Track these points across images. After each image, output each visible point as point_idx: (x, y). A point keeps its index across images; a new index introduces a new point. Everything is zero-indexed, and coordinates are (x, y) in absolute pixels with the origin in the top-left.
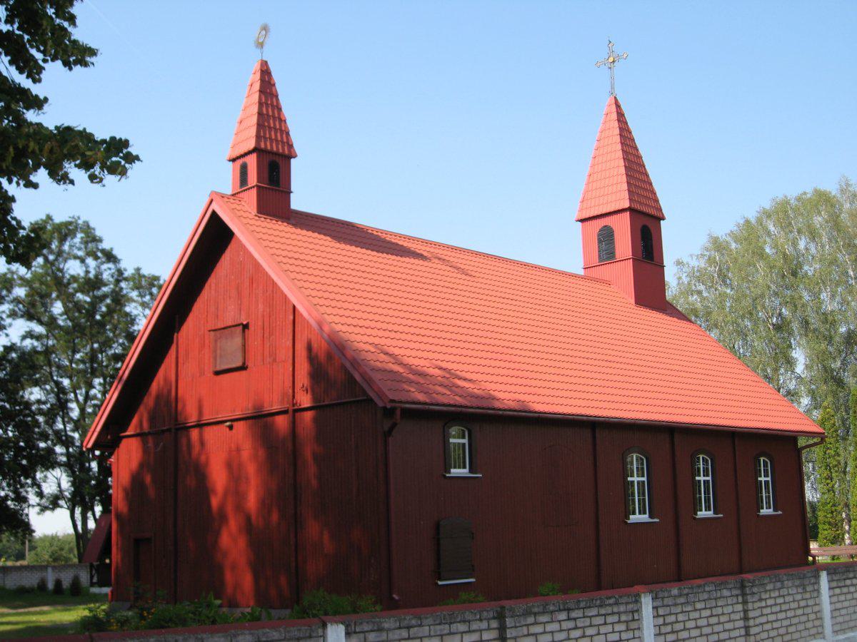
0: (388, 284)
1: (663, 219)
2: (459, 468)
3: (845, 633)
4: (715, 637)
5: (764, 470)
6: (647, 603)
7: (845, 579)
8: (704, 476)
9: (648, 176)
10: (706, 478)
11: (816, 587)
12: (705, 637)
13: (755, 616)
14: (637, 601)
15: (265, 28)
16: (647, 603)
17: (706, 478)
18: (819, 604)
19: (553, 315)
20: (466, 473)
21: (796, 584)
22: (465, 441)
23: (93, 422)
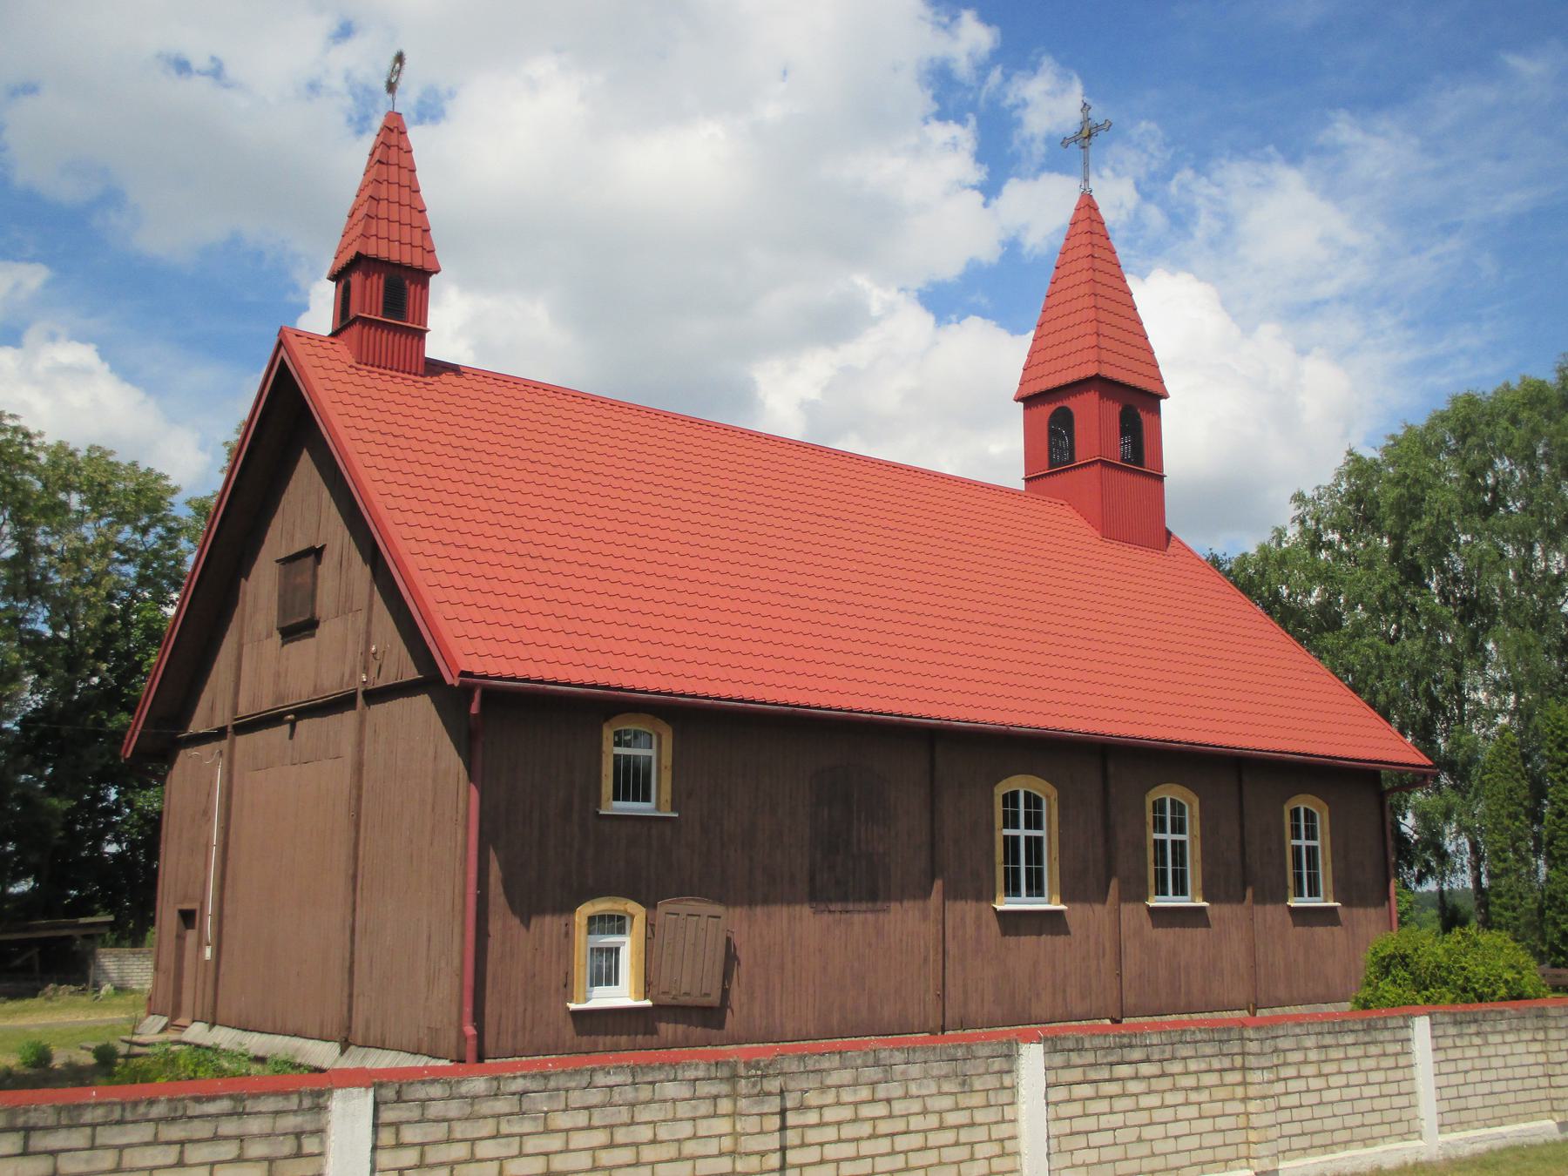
0: (975, 538)
1: (1166, 397)
2: (636, 799)
3: (1517, 1121)
4: (864, 1167)
5: (1306, 827)
6: (1032, 1058)
7: (1111, 1064)
8: (1307, 838)
9: (1140, 324)
10: (1295, 842)
11: (1007, 1081)
12: (833, 1166)
13: (764, 1148)
14: (1011, 1057)
15: (400, 58)
16: (1032, 1058)
17: (1295, 842)
18: (1013, 1121)
19: (904, 545)
20: (651, 810)
21: (935, 1072)
22: (652, 753)
23: (1408, 771)
